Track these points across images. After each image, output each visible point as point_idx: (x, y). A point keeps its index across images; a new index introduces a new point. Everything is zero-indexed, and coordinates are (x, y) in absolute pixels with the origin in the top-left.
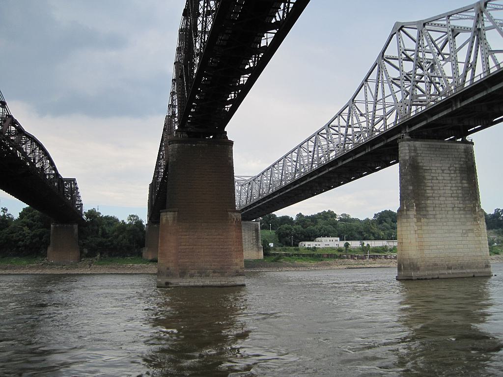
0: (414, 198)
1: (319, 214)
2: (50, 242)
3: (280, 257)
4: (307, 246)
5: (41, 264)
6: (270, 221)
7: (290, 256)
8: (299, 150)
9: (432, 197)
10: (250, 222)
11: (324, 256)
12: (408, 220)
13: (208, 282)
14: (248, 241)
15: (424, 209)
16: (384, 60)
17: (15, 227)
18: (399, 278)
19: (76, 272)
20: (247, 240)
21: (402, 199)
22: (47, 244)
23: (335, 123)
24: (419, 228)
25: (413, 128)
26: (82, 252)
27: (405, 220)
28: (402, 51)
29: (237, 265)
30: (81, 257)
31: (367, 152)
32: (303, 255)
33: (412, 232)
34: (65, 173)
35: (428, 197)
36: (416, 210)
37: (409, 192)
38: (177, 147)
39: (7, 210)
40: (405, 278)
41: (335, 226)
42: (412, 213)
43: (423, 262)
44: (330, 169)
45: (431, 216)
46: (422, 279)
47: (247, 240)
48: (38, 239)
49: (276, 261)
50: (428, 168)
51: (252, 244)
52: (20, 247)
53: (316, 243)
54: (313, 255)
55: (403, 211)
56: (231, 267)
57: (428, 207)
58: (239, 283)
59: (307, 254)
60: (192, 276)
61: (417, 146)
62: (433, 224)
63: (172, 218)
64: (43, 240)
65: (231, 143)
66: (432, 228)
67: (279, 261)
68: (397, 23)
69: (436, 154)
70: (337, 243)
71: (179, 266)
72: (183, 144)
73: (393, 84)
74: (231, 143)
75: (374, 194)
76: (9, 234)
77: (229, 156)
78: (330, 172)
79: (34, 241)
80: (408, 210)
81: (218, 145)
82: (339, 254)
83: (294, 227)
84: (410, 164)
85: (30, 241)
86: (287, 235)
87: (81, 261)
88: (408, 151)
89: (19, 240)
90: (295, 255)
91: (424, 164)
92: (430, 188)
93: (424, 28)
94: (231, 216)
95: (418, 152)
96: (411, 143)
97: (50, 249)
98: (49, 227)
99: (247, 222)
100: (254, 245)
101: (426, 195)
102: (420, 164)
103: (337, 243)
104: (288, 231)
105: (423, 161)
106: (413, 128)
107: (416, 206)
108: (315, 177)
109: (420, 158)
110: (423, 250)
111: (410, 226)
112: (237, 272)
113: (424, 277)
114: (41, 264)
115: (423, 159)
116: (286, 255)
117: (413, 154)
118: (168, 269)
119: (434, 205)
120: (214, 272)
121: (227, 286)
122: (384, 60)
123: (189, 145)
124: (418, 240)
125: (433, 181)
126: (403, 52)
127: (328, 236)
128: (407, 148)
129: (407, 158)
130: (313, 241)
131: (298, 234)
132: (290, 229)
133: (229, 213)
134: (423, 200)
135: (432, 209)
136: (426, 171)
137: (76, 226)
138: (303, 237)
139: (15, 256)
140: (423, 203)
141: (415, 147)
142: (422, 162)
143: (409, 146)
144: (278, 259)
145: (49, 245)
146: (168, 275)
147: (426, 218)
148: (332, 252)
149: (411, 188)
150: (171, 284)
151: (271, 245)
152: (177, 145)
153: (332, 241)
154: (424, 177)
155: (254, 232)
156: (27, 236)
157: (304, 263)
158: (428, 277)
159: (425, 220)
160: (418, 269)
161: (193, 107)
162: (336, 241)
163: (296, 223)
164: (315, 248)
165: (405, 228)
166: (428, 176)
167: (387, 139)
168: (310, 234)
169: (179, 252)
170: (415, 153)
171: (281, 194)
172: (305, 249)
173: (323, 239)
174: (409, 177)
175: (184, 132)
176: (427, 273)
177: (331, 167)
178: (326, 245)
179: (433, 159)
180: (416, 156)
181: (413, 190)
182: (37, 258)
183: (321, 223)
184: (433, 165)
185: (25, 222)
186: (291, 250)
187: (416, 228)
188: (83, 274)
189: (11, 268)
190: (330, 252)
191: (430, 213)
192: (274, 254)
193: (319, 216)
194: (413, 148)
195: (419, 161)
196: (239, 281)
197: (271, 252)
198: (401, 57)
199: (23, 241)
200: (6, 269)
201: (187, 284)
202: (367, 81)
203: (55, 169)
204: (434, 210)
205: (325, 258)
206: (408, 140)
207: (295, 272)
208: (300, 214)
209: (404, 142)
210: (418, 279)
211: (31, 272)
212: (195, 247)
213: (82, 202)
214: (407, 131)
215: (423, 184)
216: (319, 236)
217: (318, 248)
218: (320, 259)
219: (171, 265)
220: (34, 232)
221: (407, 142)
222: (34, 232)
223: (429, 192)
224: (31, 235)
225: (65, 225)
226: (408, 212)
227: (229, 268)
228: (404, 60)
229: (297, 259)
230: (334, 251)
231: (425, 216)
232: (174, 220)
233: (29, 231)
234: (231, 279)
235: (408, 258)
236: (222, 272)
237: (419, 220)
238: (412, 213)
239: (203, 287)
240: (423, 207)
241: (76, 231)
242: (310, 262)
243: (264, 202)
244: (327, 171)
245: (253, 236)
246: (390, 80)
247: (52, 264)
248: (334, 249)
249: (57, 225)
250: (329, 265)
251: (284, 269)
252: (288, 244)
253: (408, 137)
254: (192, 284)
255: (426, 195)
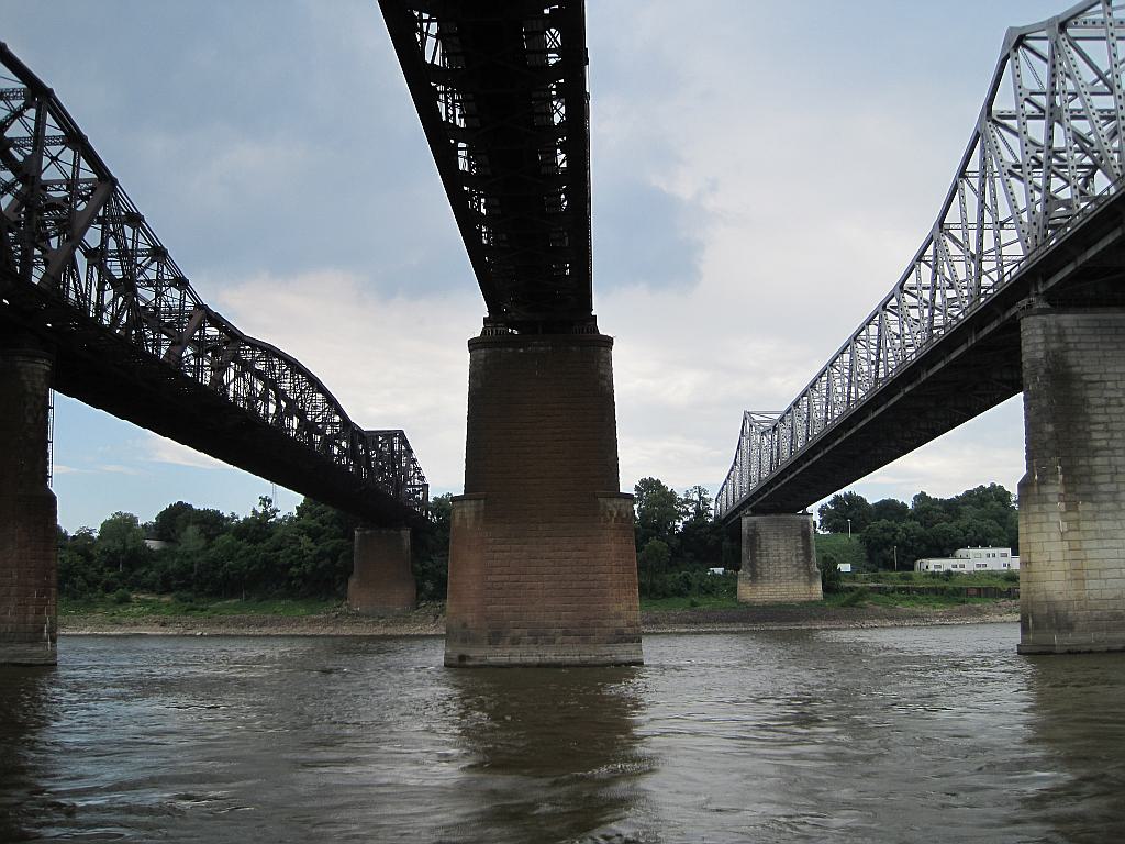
0: (1057, 453)
1: (969, 493)
2: (353, 566)
3: (862, 594)
4: (932, 569)
5: (334, 615)
6: (852, 513)
7: (887, 594)
8: (852, 348)
9: (1108, 449)
10: (792, 516)
11: (971, 592)
12: (1045, 506)
13: (550, 655)
14: (786, 560)
15: (1086, 479)
16: (994, 121)
17: (283, 538)
18: (1024, 650)
19: (404, 631)
20: (783, 558)
21: (1031, 455)
22: (347, 572)
23: (912, 281)
24: (1073, 526)
25: (1051, 283)
26: (420, 589)
27: (1036, 508)
28: (1023, 97)
29: (618, 616)
30: (419, 599)
31: (969, 345)
32: (921, 591)
33: (1055, 536)
34: (367, 417)
35: (1097, 449)
36: (1064, 483)
37: (1047, 438)
38: (483, 356)
39: (270, 501)
40: (1038, 649)
41: (1004, 521)
42: (1055, 489)
43: (1082, 609)
44: (907, 390)
45: (1105, 497)
46: (1079, 652)
47: (783, 558)
48: (328, 561)
49: (851, 603)
50: (1096, 378)
51: (795, 566)
52: (291, 579)
53: (954, 562)
54: (943, 590)
55: (1032, 485)
56: (605, 623)
57: (1096, 474)
58: (624, 658)
59: (929, 588)
60: (515, 642)
61: (1065, 324)
62: (1109, 516)
63: (473, 515)
64: (337, 564)
65: (608, 342)
66: (1105, 525)
67: (860, 603)
68: (1011, 29)
69: (1104, 350)
70: (1006, 560)
71: (487, 619)
72: (498, 350)
73: (1012, 179)
74: (608, 342)
75: (982, 452)
76: (270, 551)
77: (602, 372)
78: (907, 395)
79: (320, 566)
80: (1042, 483)
81: (574, 349)
82: (1005, 586)
83: (903, 525)
84: (1048, 371)
85: (313, 567)
86: (887, 544)
87: (418, 608)
88: (1041, 340)
89: (291, 564)
90: (900, 590)
91: (1086, 370)
92: (1101, 427)
93: (1063, 36)
94: (605, 506)
95: (1069, 339)
96: (1051, 319)
97: (353, 581)
98: (352, 538)
99: (783, 516)
100: (800, 568)
101: (1090, 444)
102: (1076, 369)
103: (1006, 560)
104: (888, 536)
105: (1081, 362)
106: (1051, 283)
107: (1062, 472)
108: (883, 409)
109: (1073, 353)
110: (1084, 580)
111: (1048, 521)
112: (620, 633)
113: (1087, 648)
114: (334, 615)
115: (1082, 357)
116: (879, 590)
117: (1054, 346)
118: (465, 625)
119: (1113, 470)
120: (566, 633)
121: (595, 666)
122: (994, 121)
123: (510, 350)
124: (1069, 556)
125: (1108, 410)
126: (1027, 99)
127: (985, 546)
128: (1039, 331)
129: (1040, 355)
130: (947, 556)
131: (912, 540)
132: (894, 529)
133: (601, 500)
134: (1081, 457)
135: (1106, 478)
136: (1089, 385)
137: (406, 533)
138: (923, 547)
139: (283, 597)
140: (1082, 466)
141: (1059, 327)
142: (1078, 365)
143: (1044, 325)
144: (856, 599)
145: (350, 573)
146: (464, 641)
147: (1092, 502)
148: (991, 582)
149: (1050, 428)
150: (469, 658)
151: (845, 567)
152: (483, 351)
153: (994, 555)
154: (1084, 400)
155: (800, 538)
156: (308, 555)
157: (920, 609)
158: (1094, 648)
159: (1089, 506)
160: (1070, 627)
161: (19, 257)
162: (1005, 555)
163: (910, 517)
164: (949, 573)
165: (1035, 528)
166: (1094, 397)
167: (1004, 313)
168: (941, 540)
169: (489, 588)
170: (1061, 341)
171: (826, 451)
172: (926, 576)
173: (972, 552)
174: (1044, 403)
175: (502, 322)
176: (1092, 637)
177: (910, 383)
178: (978, 566)
179: (1109, 354)
180: (1063, 351)
181: (1056, 435)
182: (329, 601)
183: (969, 515)
184: (1108, 370)
185: (303, 527)
186: (893, 578)
187: (1064, 526)
188: (401, 637)
189: (272, 623)
190: (985, 583)
191: (1102, 488)
192: (851, 589)
193: (968, 498)
194: (1055, 331)
195: (1073, 361)
196: (622, 653)
197: (843, 584)
198: (1022, 111)
199: (299, 565)
200: (262, 625)
201: (504, 660)
202: (965, 177)
203: (340, 411)
204: (1112, 482)
205: (971, 596)
206: (1042, 312)
207: (895, 631)
208: (923, 494)
209: (1031, 318)
210: (1069, 652)
211: (310, 632)
212: (522, 577)
213: (427, 481)
214: (1041, 290)
215: (1081, 418)
216: (964, 547)
217: (958, 574)
218: (961, 599)
219: (469, 617)
220: (320, 547)
221: (1039, 317)
222: (320, 547)
223: (1099, 439)
224: (314, 552)
225: (384, 532)
226: (1043, 489)
227: (599, 625)
228: (1029, 117)
229: (902, 599)
230: (996, 580)
231: (1088, 497)
232: (477, 518)
233: (312, 545)
234: (605, 650)
235: (1043, 599)
236: (583, 634)
237: (1071, 506)
238: (1055, 489)
239: (539, 666)
240: (1081, 475)
241: (407, 542)
242: (934, 607)
243: (799, 471)
244: (901, 394)
245: (797, 548)
246: (1005, 170)
247: (358, 614)
248: (997, 576)
249: (367, 532)
250: (979, 612)
251: (868, 623)
252: (888, 565)
253: (1043, 305)
254: (515, 660)
255: (1090, 444)
